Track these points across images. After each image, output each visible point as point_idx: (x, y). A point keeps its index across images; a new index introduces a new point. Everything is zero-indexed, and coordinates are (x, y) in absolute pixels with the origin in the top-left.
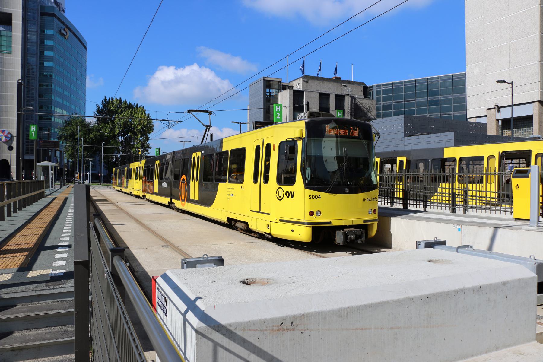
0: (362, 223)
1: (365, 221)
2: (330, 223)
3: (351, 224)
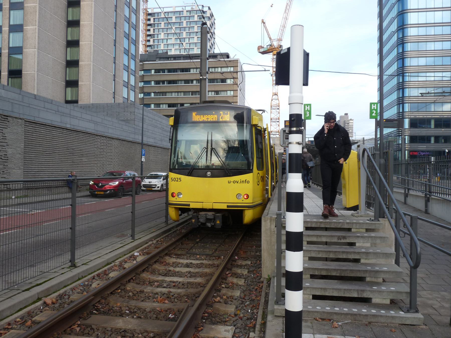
0: (226, 208)
1: (228, 206)
2: (189, 205)
3: (211, 208)
